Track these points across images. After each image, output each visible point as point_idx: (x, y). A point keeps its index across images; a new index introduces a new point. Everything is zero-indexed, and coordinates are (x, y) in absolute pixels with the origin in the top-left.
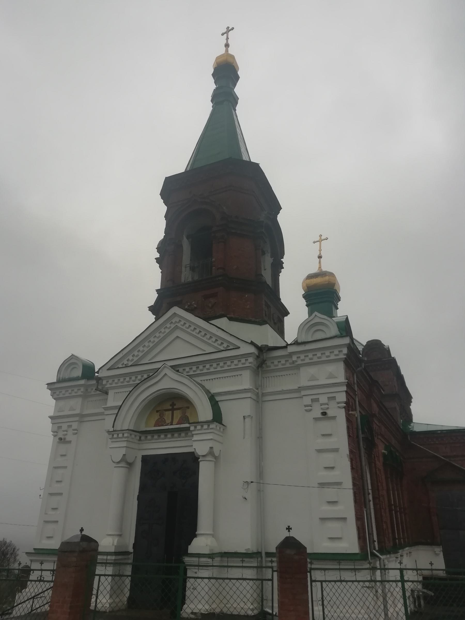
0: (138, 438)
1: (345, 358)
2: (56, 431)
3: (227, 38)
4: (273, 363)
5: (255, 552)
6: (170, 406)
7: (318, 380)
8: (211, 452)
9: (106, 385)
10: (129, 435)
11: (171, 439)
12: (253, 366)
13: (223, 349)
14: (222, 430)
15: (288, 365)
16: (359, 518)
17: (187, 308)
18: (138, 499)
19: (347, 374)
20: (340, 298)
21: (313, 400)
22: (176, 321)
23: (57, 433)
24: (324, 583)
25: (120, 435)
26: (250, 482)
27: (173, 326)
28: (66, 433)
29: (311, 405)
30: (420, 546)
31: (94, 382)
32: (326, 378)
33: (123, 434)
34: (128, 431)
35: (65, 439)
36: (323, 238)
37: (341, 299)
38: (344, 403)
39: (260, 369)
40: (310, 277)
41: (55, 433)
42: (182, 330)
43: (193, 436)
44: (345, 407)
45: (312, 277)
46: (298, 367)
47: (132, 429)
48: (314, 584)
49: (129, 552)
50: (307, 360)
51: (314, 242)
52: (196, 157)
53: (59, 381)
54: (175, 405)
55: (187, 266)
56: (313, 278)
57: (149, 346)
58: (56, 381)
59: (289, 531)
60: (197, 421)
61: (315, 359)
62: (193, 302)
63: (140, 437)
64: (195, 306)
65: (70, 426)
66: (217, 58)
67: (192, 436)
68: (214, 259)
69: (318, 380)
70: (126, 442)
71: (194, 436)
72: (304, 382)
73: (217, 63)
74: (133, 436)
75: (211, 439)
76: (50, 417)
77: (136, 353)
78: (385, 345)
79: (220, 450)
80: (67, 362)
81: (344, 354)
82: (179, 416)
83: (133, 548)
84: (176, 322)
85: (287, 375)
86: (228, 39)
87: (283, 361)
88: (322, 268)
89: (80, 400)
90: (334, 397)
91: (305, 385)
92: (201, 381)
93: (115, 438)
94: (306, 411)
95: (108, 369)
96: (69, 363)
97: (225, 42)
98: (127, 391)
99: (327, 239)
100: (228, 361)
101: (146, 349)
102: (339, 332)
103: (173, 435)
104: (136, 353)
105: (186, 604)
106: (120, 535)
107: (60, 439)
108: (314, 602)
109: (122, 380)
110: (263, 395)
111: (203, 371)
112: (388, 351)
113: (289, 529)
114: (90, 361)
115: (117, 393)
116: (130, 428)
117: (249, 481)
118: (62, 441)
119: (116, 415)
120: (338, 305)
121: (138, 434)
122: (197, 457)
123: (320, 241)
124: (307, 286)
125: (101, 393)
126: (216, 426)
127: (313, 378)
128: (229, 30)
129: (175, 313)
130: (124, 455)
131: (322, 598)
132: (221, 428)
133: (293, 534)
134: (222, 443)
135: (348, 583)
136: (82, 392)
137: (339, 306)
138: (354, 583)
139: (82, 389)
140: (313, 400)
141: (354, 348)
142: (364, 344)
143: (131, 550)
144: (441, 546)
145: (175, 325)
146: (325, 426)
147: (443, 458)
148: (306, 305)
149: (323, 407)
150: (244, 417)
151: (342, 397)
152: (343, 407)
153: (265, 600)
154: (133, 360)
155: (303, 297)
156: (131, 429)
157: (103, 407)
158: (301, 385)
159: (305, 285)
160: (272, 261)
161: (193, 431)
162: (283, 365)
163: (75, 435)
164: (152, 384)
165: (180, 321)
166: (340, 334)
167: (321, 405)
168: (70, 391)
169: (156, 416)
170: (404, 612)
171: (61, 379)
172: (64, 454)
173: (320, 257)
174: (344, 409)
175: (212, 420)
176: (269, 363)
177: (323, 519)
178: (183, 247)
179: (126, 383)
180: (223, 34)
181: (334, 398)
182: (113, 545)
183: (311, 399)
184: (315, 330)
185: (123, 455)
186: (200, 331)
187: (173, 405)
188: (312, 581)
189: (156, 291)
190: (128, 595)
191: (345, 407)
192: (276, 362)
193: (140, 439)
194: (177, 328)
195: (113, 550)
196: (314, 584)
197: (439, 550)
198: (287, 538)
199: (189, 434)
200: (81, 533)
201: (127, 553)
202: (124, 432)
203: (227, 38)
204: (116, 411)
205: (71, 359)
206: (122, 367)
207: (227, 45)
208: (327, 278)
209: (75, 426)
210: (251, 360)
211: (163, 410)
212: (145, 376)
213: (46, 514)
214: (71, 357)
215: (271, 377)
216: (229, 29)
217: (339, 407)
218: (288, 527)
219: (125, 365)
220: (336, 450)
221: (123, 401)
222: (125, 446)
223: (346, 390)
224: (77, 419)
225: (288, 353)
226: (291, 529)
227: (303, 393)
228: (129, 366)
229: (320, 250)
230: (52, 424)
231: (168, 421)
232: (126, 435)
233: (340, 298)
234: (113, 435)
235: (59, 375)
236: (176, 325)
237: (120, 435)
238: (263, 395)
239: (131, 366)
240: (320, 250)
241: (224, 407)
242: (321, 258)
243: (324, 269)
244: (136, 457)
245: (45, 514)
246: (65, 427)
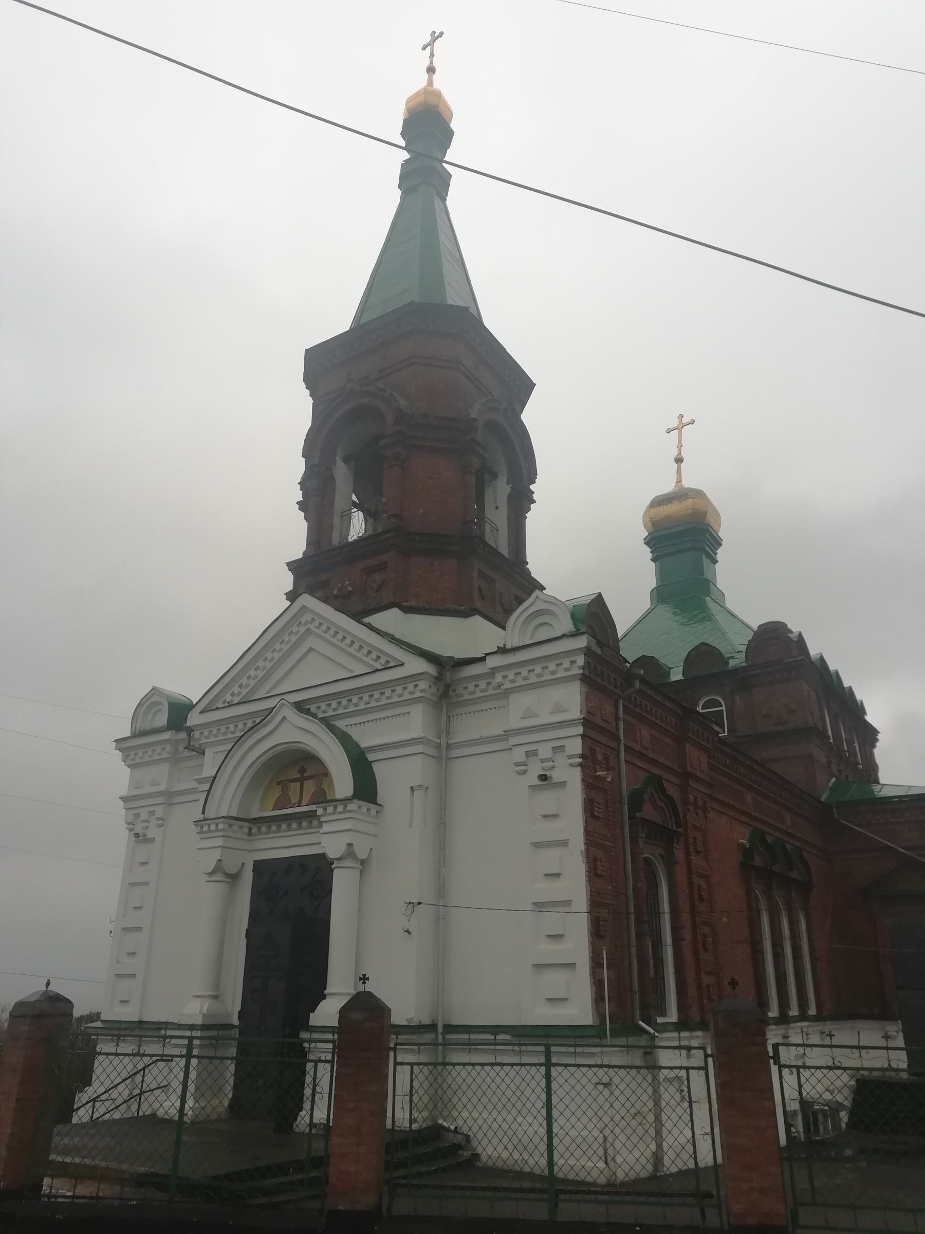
0: (246, 830)
1: (582, 674)
2: (131, 822)
3: (432, 55)
4: (466, 688)
5: (427, 1023)
6: (298, 773)
7: (538, 716)
8: (350, 853)
9: (199, 739)
10: (227, 826)
11: (297, 830)
12: (429, 696)
13: (380, 668)
14: (373, 812)
15: (491, 691)
16: (596, 964)
17: (336, 594)
18: (246, 937)
19: (589, 704)
20: (719, 540)
21: (528, 754)
22: (307, 621)
23: (134, 824)
24: (417, 1066)
25: (213, 827)
26: (417, 904)
27: (302, 629)
28: (146, 824)
29: (525, 762)
30: (857, 1021)
31: (183, 735)
32: (551, 713)
33: (217, 825)
34: (222, 820)
35: (145, 835)
36: (685, 421)
37: (723, 543)
38: (580, 758)
39: (443, 701)
40: (658, 502)
41: (131, 824)
42: (318, 636)
43: (322, 827)
44: (580, 765)
45: (661, 503)
46: (507, 693)
47: (235, 815)
48: (398, 1067)
49: (232, 1024)
50: (520, 682)
51: (669, 431)
52: (366, 302)
53: (134, 735)
54: (306, 770)
55: (345, 514)
56: (664, 504)
57: (266, 668)
58: (130, 735)
59: (364, 983)
60: (333, 798)
61: (533, 679)
62: (347, 583)
63: (250, 829)
64: (350, 589)
65: (152, 813)
66: (409, 100)
67: (320, 825)
68: (386, 499)
69: (538, 716)
70: (221, 839)
71: (324, 825)
72: (515, 722)
73: (408, 110)
74: (235, 828)
75: (350, 830)
76: (122, 798)
77: (244, 681)
78: (794, 631)
79: (371, 849)
80: (146, 701)
81: (580, 668)
82: (312, 790)
83: (239, 1018)
84: (307, 622)
85: (491, 709)
86: (433, 56)
87: (483, 685)
88: (683, 484)
89: (166, 767)
90: (563, 746)
91: (514, 727)
92: (347, 726)
93: (206, 832)
94: (518, 773)
95: (201, 712)
96: (149, 702)
97: (427, 63)
98: (224, 751)
99: (693, 422)
100: (388, 689)
101: (261, 674)
102: (573, 626)
103: (300, 824)
104: (244, 681)
105: (303, 1110)
106: (216, 997)
107: (137, 835)
108: (328, 1091)
109: (232, 728)
110: (449, 747)
111: (348, 708)
112: (800, 643)
113: (364, 979)
114: (186, 697)
115: (217, 752)
116: (231, 815)
117: (416, 901)
118: (141, 838)
119: (206, 793)
120: (716, 554)
121: (246, 824)
122: (330, 861)
123: (680, 428)
124: (651, 521)
125: (194, 753)
126: (359, 807)
127: (529, 713)
128: (435, 37)
129: (304, 606)
130: (220, 861)
131: (411, 1091)
132: (372, 810)
133: (369, 987)
134: (376, 836)
135: (476, 1067)
136: (168, 753)
137: (718, 557)
138: (466, 1067)
139: (168, 748)
140: (528, 754)
141: (605, 655)
142: (755, 627)
143: (236, 1022)
144: (900, 1022)
145: (306, 627)
146: (547, 800)
147: (903, 850)
148: (652, 560)
149: (545, 764)
150: (412, 788)
151: (576, 747)
152: (578, 763)
153: (318, 1093)
154: (241, 693)
155: (645, 544)
156: (233, 816)
157: (195, 778)
158: (508, 727)
159: (648, 520)
160: (510, 491)
161: (322, 816)
162: (482, 691)
163: (160, 828)
164: (264, 734)
165: (313, 620)
166: (575, 629)
167: (542, 761)
168: (150, 753)
169: (276, 792)
170: (545, 1116)
171: (137, 732)
172: (145, 861)
173: (679, 460)
174: (579, 768)
175: (352, 795)
176: (460, 689)
177: (539, 967)
178: (335, 479)
179: (221, 737)
180: (424, 48)
181: (534, 753)
182: (200, 1012)
183: (526, 752)
184: (538, 625)
185: (218, 860)
186: (344, 636)
187: (302, 770)
188: (396, 1064)
189: (287, 565)
190: (230, 1095)
191: (580, 765)
192: (471, 687)
193: (250, 834)
194: (309, 632)
195: (199, 1021)
196: (398, 1067)
197: (895, 1029)
198: (358, 994)
199: (315, 823)
200: (47, 988)
201: (230, 1027)
202: (218, 820)
203: (432, 55)
204: (207, 787)
205: (152, 695)
206: (223, 706)
207: (431, 70)
208: (689, 502)
209: (159, 811)
210: (423, 685)
211: (287, 780)
212: (250, 724)
213: (118, 962)
214: (152, 692)
215: (457, 715)
216: (436, 35)
217: (571, 765)
218: (366, 977)
219: (228, 703)
220: (564, 843)
221: (217, 770)
222: (220, 845)
223: (581, 733)
224: (161, 800)
225: (489, 669)
226: (368, 979)
227: (513, 741)
228: (235, 704)
229: (680, 446)
230: (126, 809)
231: (295, 800)
232: (221, 826)
233: (722, 540)
234: (202, 827)
235: (134, 724)
236: (308, 628)
237: (213, 827)
238: (449, 747)
239: (239, 703)
240: (680, 446)
241: (379, 770)
242: (681, 463)
243: (687, 483)
244: (243, 864)
245: (117, 963)
246: (144, 814)
